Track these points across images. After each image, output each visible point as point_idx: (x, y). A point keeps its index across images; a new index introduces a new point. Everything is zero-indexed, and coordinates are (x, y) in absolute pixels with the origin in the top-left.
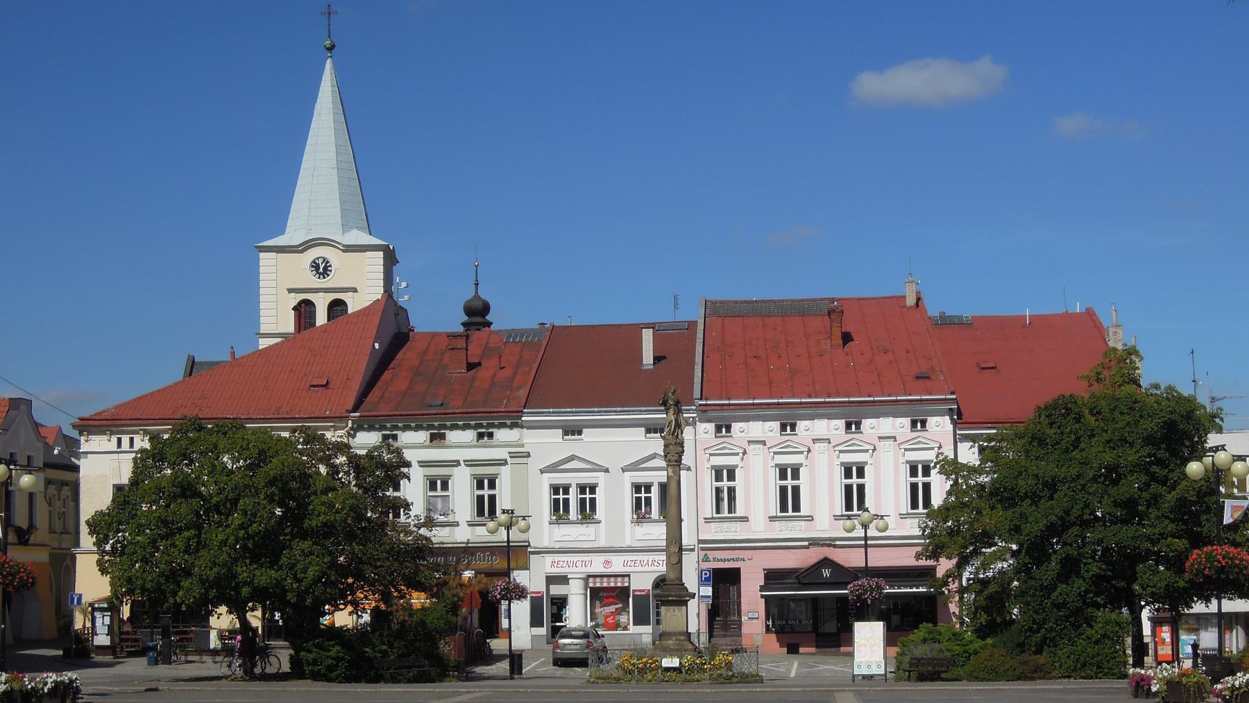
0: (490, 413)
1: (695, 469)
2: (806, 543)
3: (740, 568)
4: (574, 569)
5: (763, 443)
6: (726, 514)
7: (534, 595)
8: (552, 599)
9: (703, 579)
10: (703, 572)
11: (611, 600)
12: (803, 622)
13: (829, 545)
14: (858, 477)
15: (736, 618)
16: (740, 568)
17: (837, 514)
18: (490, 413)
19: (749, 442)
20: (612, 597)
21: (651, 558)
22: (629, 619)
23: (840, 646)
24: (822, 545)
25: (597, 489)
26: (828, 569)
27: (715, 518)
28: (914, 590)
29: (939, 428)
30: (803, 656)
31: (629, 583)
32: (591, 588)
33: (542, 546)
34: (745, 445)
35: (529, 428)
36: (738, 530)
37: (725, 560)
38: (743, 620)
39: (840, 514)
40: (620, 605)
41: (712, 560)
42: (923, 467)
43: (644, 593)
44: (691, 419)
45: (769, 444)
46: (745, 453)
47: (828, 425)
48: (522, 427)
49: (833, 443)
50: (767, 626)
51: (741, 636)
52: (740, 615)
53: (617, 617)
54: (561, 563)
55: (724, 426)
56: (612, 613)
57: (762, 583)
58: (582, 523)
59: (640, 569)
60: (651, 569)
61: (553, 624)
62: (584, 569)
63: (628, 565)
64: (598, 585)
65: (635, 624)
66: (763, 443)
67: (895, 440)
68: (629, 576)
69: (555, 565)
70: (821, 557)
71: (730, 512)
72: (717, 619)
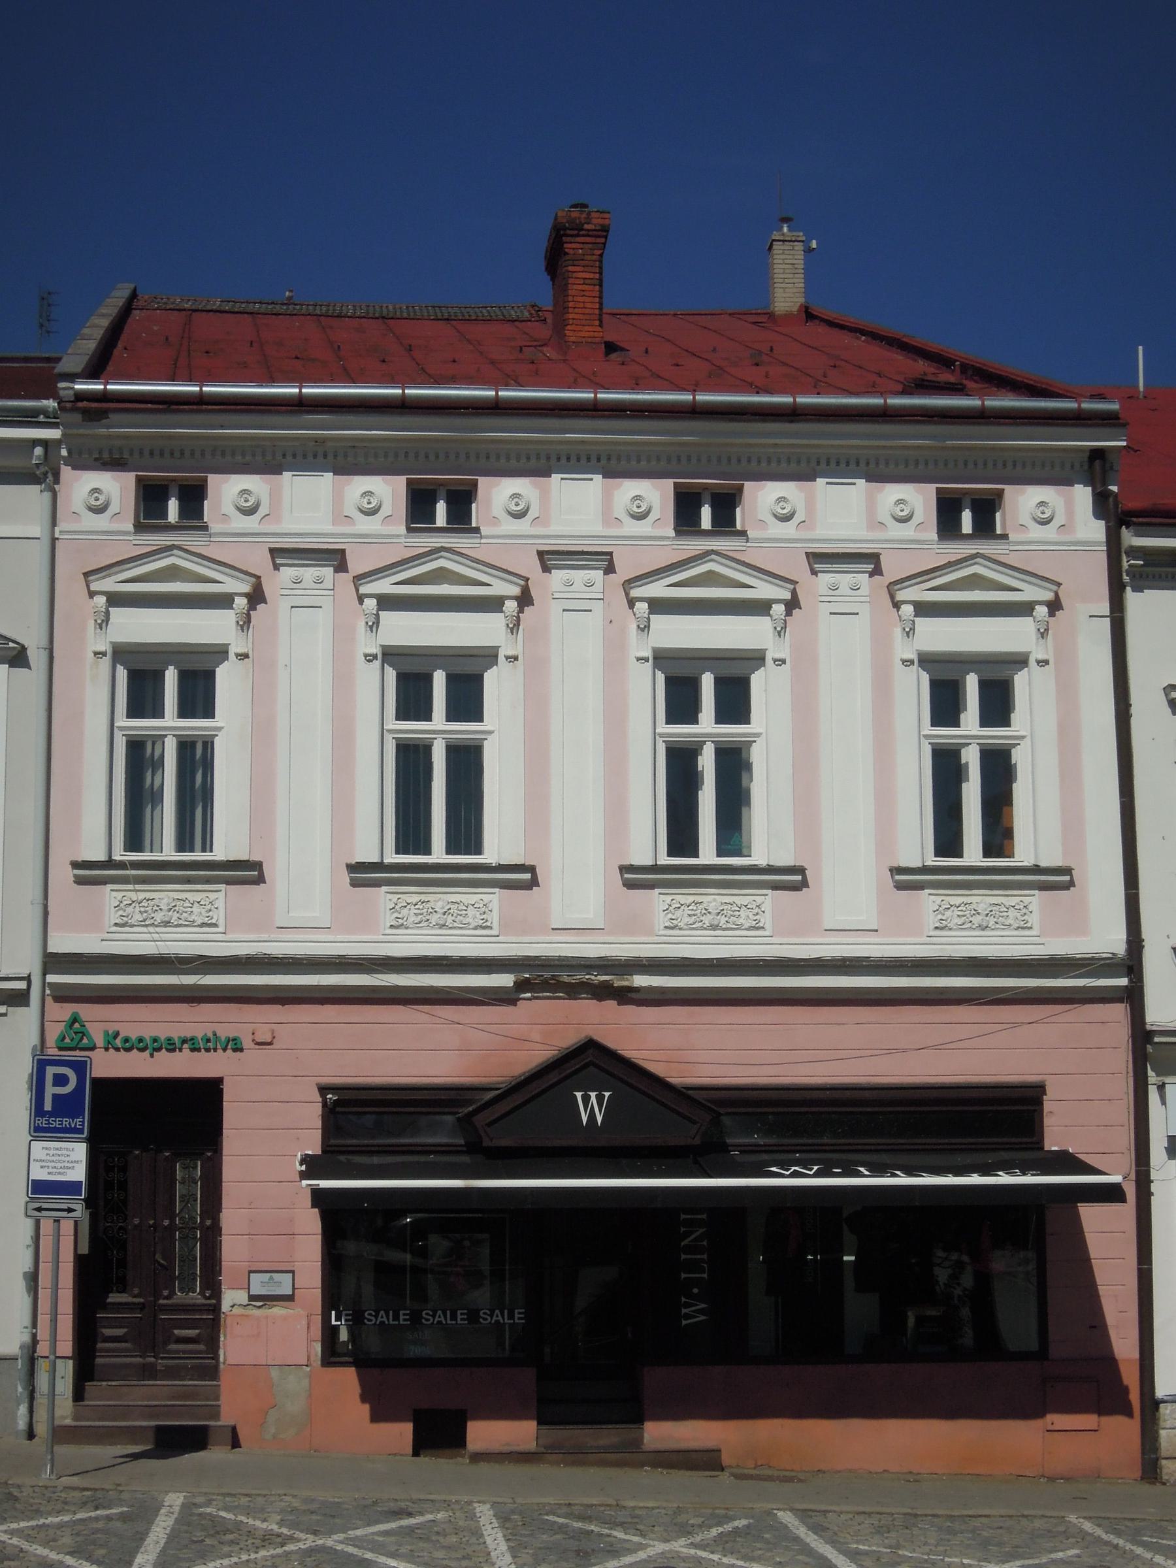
1: (44, 655)
2: (506, 980)
3: (54, 1074)
5: (337, 559)
6: (169, 852)
9: (48, 1106)
10: (50, 1071)
12: (486, 1319)
13: (603, 992)
14: (453, 714)
15: (195, 1297)
16: (54, 1074)
17: (904, 863)
19: (274, 552)
23: (638, 1419)
24: (573, 991)
26: (600, 1089)
27: (122, 865)
28: (975, 1179)
29: (1049, 533)
30: (484, 1468)
34: (259, 562)
36: (494, 919)
37: (155, 1046)
38: (225, 1306)
39: (101, 856)
41: (100, 1041)
42: (453, 680)
44: (38, 451)
45: (357, 565)
46: (256, 597)
47: (338, 498)
49: (625, 570)
50: (330, 1334)
51: (211, 1371)
52: (213, 1287)
55: (174, 489)
57: (314, 1147)
66: (337, 559)
67: (877, 571)
70: (569, 1039)
71: (184, 843)
72: (113, 1298)
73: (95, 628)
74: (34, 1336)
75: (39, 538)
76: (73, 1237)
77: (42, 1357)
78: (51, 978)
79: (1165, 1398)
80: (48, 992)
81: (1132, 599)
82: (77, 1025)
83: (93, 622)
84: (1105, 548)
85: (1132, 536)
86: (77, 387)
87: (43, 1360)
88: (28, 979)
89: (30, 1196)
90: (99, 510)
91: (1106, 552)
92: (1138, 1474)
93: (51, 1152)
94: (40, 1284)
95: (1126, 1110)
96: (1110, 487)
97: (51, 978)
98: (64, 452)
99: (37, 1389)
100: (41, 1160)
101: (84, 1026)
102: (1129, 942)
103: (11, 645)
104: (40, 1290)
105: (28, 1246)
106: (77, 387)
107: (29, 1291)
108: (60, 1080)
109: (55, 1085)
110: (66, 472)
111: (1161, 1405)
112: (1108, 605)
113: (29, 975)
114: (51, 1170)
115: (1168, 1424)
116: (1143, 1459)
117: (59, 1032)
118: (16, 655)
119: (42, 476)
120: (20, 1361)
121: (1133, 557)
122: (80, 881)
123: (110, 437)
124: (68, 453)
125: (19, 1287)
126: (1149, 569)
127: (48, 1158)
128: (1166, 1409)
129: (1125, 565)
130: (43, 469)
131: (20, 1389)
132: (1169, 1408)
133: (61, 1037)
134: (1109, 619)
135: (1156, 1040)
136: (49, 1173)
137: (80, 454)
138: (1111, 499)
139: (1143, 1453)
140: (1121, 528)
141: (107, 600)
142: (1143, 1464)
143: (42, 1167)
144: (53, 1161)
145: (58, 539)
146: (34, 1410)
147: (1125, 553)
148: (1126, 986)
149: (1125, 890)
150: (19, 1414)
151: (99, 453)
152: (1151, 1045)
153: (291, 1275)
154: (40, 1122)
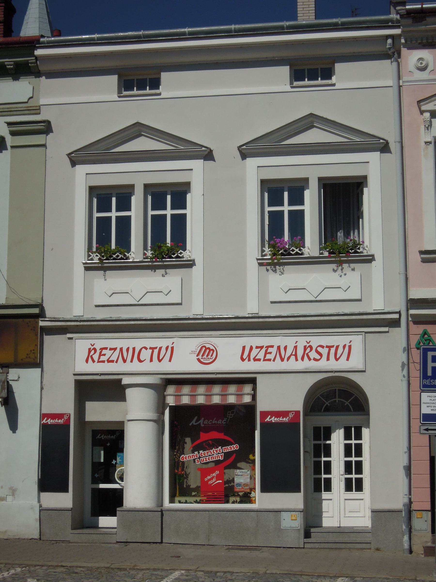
0: (11, 111)
1: (399, 145)
4: (135, 366)
7: (50, 421)
8: (95, 433)
9: (430, 373)
11: (215, 435)
18: (11, 111)
20: (218, 429)
21: (302, 342)
22: (252, 478)
25: (189, 196)
31: (254, 397)
32: (171, 407)
33: (68, 316)
35: (51, 75)
40: (235, 447)
43: (285, 420)
44: (390, 41)
48: (38, 74)
53: (228, 473)
54: (108, 353)
56: (217, 462)
58: (154, 268)
59: (278, 365)
60: (306, 364)
61: (95, 486)
62: (155, 366)
63: (252, 357)
64: (186, 400)
65: (265, 489)
68: (253, 381)
69: (96, 357)
73: (425, 130)
74: (410, 499)
75: (392, 87)
76: (429, 447)
77: (415, 510)
78: (412, 312)
80: (410, 319)
82: (426, 336)
83: (423, 126)
86: (407, 7)
87: (415, 512)
88: (399, 313)
89: (422, 422)
90: (423, 69)
93: (433, 398)
94: (412, 472)
97: (412, 312)
98: (403, 41)
99: (413, 527)
100: (427, 403)
101: (430, 336)
103: (381, 141)
104: (412, 475)
105: (405, 452)
106: (407, 7)
107: (407, 476)
110: (404, 51)
113: (400, 311)
114: (432, 408)
117: (417, 340)
118: (384, 147)
119: (391, 54)
120: (403, 512)
122: (424, 261)
123: (426, 31)
124: (405, 41)
125: (402, 473)
127: (431, 401)
130: (392, 50)
131: (404, 527)
133: (419, 342)
136: (432, 410)
137: (411, 41)
141: (430, 115)
143: (428, 407)
144: (434, 403)
145: (401, 86)
146: (412, 538)
150: (404, 540)
151: (421, 40)
153: (160, 541)
154: (425, 382)
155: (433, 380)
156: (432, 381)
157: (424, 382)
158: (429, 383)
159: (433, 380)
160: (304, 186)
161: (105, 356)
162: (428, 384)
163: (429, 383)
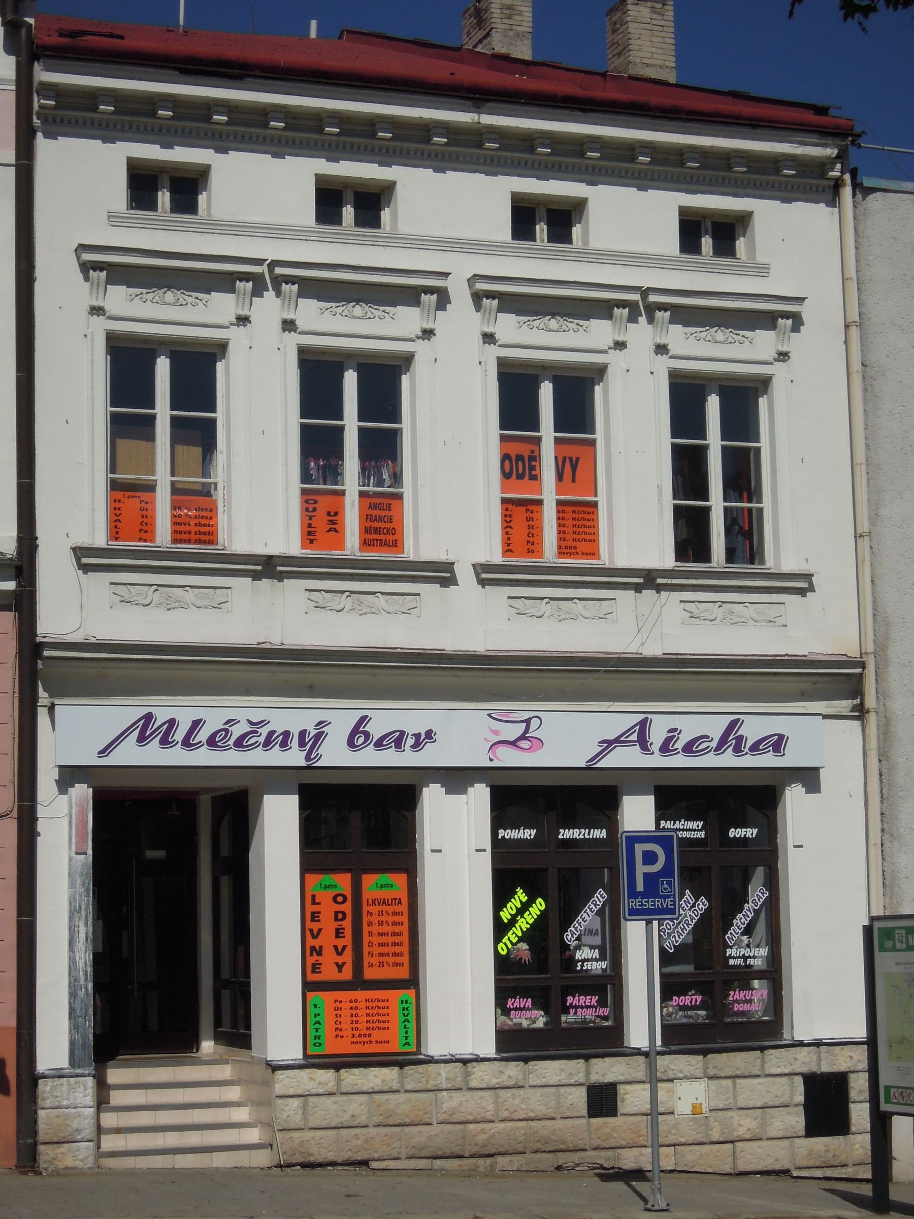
9: (640, 887)
79: (47, 1072)
81: (43, 145)
84: (14, 88)
85: (42, 70)
91: (15, 92)
92: (13, 1162)
95: (12, 736)
96: (27, 19)
102: (20, 540)
108: (649, 858)
109: (645, 862)
111: (40, 1081)
112: (14, 152)
115: (48, 1103)
116: (18, 1143)
121: (43, 96)
126: (291, 134)
128: (46, 1085)
129: (36, 106)
132: (50, 1084)
134: (14, 168)
135: (46, 653)
138: (24, 30)
139: (18, 1138)
140: (33, 65)
142: (19, 1151)
147: (36, 92)
148: (15, 591)
149: (18, 480)
152: (40, 660)
154: (659, 903)
155: (647, 900)
156: (645, 901)
157: (631, 904)
158: (639, 905)
159: (647, 900)
160: (343, 363)
161: (312, 929)
162: (637, 907)
163: (639, 905)
